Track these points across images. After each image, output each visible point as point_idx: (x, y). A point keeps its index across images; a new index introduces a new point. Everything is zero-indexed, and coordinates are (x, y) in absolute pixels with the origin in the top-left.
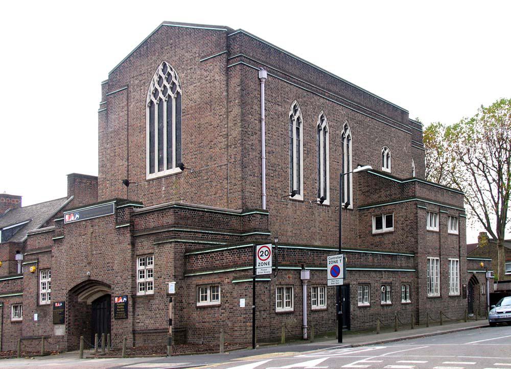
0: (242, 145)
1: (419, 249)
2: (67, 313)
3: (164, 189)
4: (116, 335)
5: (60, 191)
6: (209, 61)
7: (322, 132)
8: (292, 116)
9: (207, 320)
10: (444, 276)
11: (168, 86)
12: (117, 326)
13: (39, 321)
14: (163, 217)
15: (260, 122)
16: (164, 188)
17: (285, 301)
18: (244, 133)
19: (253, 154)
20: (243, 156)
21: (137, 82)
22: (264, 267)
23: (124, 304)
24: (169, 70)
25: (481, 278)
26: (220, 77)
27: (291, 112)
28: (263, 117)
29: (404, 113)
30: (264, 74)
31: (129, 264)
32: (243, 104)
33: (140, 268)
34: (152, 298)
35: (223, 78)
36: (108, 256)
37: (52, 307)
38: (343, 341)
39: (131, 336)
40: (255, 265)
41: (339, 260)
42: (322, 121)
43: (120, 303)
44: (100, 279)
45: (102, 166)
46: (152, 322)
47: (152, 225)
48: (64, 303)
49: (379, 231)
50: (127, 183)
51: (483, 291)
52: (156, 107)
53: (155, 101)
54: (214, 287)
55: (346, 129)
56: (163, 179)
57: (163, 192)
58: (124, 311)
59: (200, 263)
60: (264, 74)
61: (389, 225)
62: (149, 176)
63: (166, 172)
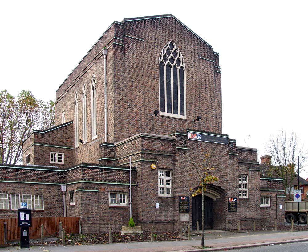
2: (226, 207)
3: (173, 126)
4: (229, 221)
6: (204, 61)
9: (265, 214)
12: (230, 216)
13: (160, 209)
14: (252, 155)
16: (174, 125)
21: (151, 41)
23: (235, 203)
34: (249, 200)
36: (223, 170)
41: (299, 192)
43: (233, 202)
46: (249, 214)
47: (246, 158)
57: (173, 128)
58: (235, 207)
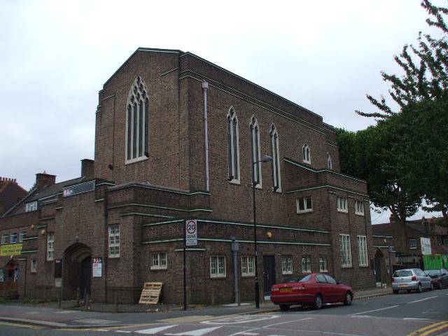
0: (189, 138)
1: (333, 228)
3: (136, 172)
5: (76, 173)
7: (254, 131)
8: (229, 117)
10: (355, 250)
11: (140, 94)
15: (204, 120)
17: (218, 268)
18: (191, 129)
19: (198, 146)
20: (190, 147)
21: (120, 91)
22: (192, 240)
24: (141, 82)
25: (385, 253)
26: (174, 87)
27: (250, 123)
28: (206, 117)
29: (319, 119)
30: (206, 85)
31: (103, 231)
32: (190, 107)
33: (111, 235)
35: (176, 87)
37: (54, 264)
38: (260, 305)
39: (104, 291)
40: (185, 238)
42: (254, 122)
44: (84, 242)
45: (96, 153)
47: (120, 200)
48: (61, 260)
49: (302, 211)
50: (111, 167)
51: (387, 262)
52: (133, 109)
53: (132, 105)
54: (162, 255)
55: (273, 129)
56: (136, 165)
59: (152, 234)
60: (206, 85)
61: (309, 207)
62: (127, 162)
63: (138, 159)
